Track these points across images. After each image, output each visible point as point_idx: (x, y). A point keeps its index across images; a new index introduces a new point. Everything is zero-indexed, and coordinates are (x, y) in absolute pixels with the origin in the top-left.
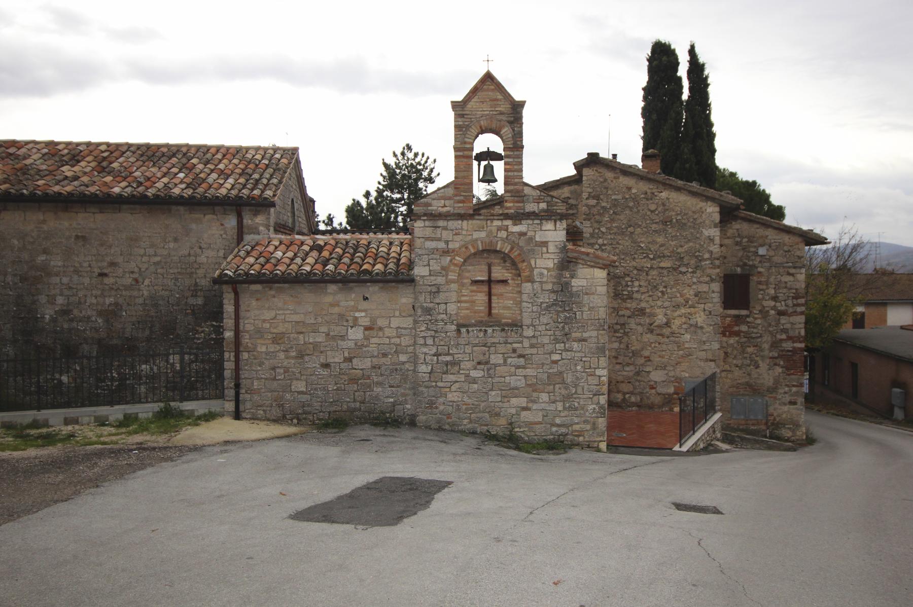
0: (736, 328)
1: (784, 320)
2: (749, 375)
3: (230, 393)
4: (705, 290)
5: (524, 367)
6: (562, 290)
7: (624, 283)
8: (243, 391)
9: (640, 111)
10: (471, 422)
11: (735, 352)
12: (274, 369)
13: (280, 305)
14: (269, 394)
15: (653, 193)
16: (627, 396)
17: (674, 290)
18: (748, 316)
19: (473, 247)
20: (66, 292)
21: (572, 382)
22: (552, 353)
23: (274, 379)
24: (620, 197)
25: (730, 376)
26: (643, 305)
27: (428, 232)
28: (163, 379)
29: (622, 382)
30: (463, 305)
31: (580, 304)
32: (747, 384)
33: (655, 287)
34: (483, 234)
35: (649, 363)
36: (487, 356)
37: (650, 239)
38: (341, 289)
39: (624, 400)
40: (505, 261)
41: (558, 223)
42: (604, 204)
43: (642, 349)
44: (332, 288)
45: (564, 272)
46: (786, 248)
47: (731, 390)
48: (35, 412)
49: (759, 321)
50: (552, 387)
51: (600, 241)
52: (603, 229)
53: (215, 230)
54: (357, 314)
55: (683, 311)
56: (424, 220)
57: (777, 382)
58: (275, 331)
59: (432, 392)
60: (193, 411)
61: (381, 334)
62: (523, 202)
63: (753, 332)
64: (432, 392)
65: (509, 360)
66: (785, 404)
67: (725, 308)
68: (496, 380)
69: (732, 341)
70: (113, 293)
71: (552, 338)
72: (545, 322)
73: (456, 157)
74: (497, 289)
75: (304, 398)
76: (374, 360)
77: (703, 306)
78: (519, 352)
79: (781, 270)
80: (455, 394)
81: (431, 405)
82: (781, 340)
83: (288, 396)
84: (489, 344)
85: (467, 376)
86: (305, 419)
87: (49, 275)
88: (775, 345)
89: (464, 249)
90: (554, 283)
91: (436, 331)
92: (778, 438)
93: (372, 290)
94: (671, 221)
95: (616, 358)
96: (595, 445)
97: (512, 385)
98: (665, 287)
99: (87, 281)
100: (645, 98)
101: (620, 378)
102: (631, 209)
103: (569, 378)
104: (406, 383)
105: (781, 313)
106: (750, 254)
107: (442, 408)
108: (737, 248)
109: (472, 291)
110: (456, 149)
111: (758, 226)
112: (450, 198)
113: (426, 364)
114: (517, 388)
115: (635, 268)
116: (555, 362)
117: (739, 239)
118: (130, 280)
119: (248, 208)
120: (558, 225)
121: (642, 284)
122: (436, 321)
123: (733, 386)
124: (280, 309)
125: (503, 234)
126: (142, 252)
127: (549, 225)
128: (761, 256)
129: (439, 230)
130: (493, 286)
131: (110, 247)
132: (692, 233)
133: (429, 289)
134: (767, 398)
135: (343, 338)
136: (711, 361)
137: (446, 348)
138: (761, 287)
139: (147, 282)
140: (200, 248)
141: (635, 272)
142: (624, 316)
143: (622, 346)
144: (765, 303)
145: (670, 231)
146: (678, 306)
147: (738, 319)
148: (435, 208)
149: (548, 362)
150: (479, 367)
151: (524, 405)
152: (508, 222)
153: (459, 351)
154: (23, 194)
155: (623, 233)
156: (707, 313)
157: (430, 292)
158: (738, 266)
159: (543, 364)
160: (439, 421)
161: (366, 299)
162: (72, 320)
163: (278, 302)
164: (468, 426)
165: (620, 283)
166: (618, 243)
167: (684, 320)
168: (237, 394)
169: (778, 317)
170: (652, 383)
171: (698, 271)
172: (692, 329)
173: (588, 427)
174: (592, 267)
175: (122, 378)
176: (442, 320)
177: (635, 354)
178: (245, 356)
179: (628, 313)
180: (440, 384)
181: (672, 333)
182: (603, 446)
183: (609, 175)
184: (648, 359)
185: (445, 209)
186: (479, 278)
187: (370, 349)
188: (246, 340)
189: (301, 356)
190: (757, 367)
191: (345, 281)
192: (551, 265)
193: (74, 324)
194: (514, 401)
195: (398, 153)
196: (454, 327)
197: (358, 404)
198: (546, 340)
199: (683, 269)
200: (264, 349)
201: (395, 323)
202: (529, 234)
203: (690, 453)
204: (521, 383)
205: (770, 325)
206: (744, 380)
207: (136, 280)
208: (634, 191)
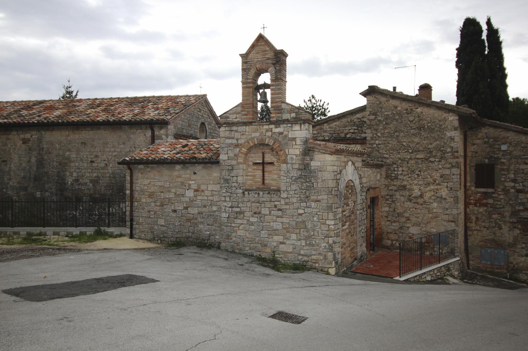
0: (485, 201)
1: (521, 196)
2: (494, 234)
3: (128, 224)
4: (447, 173)
5: (281, 217)
6: (305, 169)
7: (392, 169)
8: (135, 223)
9: (455, 64)
10: (250, 249)
11: (484, 218)
12: (149, 212)
13: (152, 176)
14: (147, 226)
15: (412, 109)
16: (394, 242)
17: (426, 173)
19: (252, 143)
20: (77, 171)
21: (311, 228)
22: (298, 208)
23: (149, 217)
24: (390, 113)
25: (480, 234)
26: (405, 183)
27: (227, 134)
28: (117, 216)
29: (391, 233)
30: (249, 177)
31: (316, 177)
32: (493, 240)
33: (413, 171)
34: (257, 134)
35: (408, 221)
36: (260, 209)
38: (182, 168)
39: (392, 245)
40: (273, 151)
41: (302, 125)
42: (379, 118)
43: (404, 212)
44: (178, 167)
45: (306, 157)
46: (523, 145)
47: (481, 243)
48: (42, 228)
49: (502, 197)
50: (298, 230)
51: (377, 142)
52: (379, 134)
53: (141, 137)
54: (190, 182)
55: (432, 187)
56: (225, 127)
57: (515, 239)
58: (150, 191)
59: (228, 229)
60: (112, 232)
61: (203, 194)
62: (281, 113)
63: (497, 204)
64: (228, 229)
65: (273, 212)
66: (522, 256)
67: (476, 187)
68: (265, 224)
69: (481, 210)
70: (96, 171)
71: (298, 199)
72: (294, 188)
73: (243, 88)
74: (268, 168)
75: (164, 229)
76: (199, 209)
77: (446, 184)
78: (278, 207)
79: (520, 161)
80: (241, 231)
81: (228, 237)
82: (519, 210)
83: (156, 227)
84: (261, 202)
85: (248, 221)
86: (164, 240)
87: (71, 162)
88: (514, 213)
89: (247, 144)
90: (300, 164)
91: (231, 193)
92: (516, 280)
93: (198, 168)
94: (424, 127)
95: (387, 217)
96: (326, 270)
97: (274, 228)
98: (420, 171)
99: (85, 165)
100: (458, 55)
101: (390, 230)
102: (397, 120)
103: (309, 226)
104: (216, 223)
105: (519, 191)
106: (495, 150)
107: (234, 239)
108: (486, 145)
109: (254, 169)
110: (243, 83)
111: (501, 130)
112: (239, 113)
113: (226, 212)
114: (277, 230)
115: (400, 159)
116: (301, 214)
117: (487, 140)
118: (104, 164)
119: (157, 125)
120: (302, 127)
121: (404, 169)
122: (231, 187)
124: (152, 179)
125: (269, 134)
126: (109, 150)
127: (297, 127)
128: (504, 151)
129: (233, 132)
130: (265, 166)
131: (95, 147)
132: (438, 135)
133: (228, 168)
134: (508, 251)
135: (183, 195)
136: (452, 222)
137: (237, 203)
138: (503, 173)
139: (111, 165)
140: (135, 147)
141: (400, 161)
142: (392, 190)
143: (391, 210)
144: (507, 184)
145: (423, 134)
146: (428, 184)
147: (486, 195)
148: (231, 119)
149: (296, 214)
150: (255, 215)
151: (282, 241)
152: (272, 126)
153: (244, 205)
154: (59, 122)
155: (392, 137)
156: (449, 189)
157: (228, 170)
158: (486, 158)
159: (293, 216)
160: (232, 247)
161: (195, 173)
162: (79, 184)
163: (151, 175)
164: (249, 251)
165: (389, 169)
166: (388, 143)
167: (432, 193)
168: (132, 225)
169: (517, 194)
170: (411, 235)
171: (443, 161)
172: (438, 199)
173: (322, 258)
174: (324, 153)
175: (100, 215)
176: (235, 187)
177: (399, 215)
178: (136, 204)
179: (395, 188)
180: (233, 225)
181: (425, 202)
182: (332, 271)
183: (383, 99)
184: (408, 219)
185: (237, 120)
186: (258, 161)
187: (197, 203)
188: (136, 195)
189: (162, 205)
190: (500, 228)
191: (183, 163)
192: (298, 153)
193: (80, 187)
194: (276, 238)
195: (307, 100)
196: (241, 191)
197: (191, 234)
198: (295, 200)
199: (432, 159)
200: (144, 201)
201: (210, 188)
202: (285, 133)
203: (407, 281)
204: (280, 227)
205: (510, 199)
206: (490, 237)
207: (106, 164)
208: (399, 109)
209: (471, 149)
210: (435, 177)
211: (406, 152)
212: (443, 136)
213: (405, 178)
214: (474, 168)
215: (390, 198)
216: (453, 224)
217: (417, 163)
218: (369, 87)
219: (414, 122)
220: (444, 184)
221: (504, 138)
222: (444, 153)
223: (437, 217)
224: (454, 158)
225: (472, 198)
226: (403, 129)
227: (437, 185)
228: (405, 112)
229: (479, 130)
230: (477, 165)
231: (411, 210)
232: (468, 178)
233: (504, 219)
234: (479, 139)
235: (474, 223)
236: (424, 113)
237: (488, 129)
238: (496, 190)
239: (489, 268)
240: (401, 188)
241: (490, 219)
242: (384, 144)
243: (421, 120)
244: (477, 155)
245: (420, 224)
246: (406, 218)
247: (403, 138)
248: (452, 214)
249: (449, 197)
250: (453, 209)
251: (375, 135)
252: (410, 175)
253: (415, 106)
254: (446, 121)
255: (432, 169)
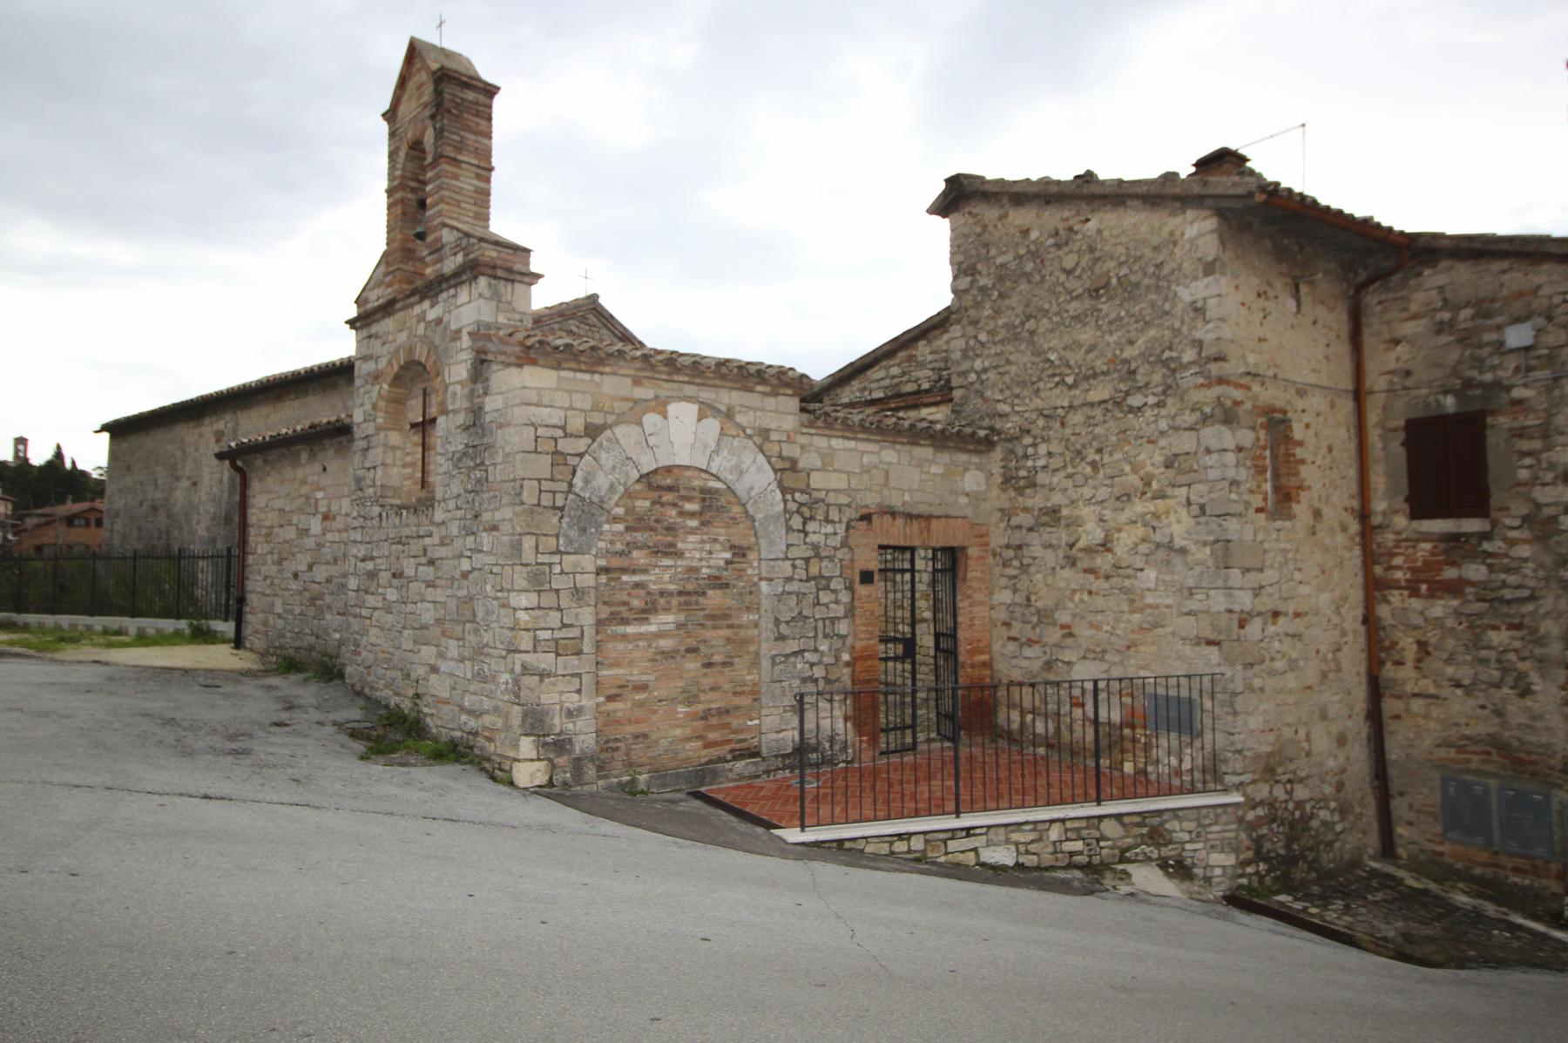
2: (1499, 713)
4: (1187, 448)
11: (1451, 643)
15: (1071, 229)
17: (1118, 456)
18: (1485, 536)
24: (1008, 257)
25: (1436, 712)
26: (1057, 499)
32: (1494, 741)
33: (1079, 453)
35: (1069, 641)
37: (1067, 339)
47: (1442, 753)
51: (978, 364)
52: (983, 337)
55: (1139, 507)
63: (1504, 585)
69: (1438, 608)
77: (1184, 490)
94: (1107, 285)
95: (1007, 624)
98: (1099, 451)
102: (1028, 277)
108: (1445, 339)
111: (1505, 264)
115: (1041, 413)
117: (1446, 316)
123: (1446, 743)
136: (1210, 643)
138: (1525, 445)
141: (1041, 422)
142: (1019, 527)
144: (1542, 495)
146: (1125, 497)
155: (1017, 338)
156: (1195, 510)
158: (1446, 393)
165: (1012, 451)
166: (1008, 362)
167: (1140, 531)
171: (1170, 401)
177: (1044, 617)
181: (1117, 567)
190: (1526, 692)
199: (1135, 401)
206: (1481, 729)
209: (1381, 363)
210: (1149, 468)
211: (1057, 384)
212: (1167, 307)
213: (1055, 480)
214: (1402, 435)
215: (1016, 557)
216: (1213, 654)
217: (1089, 421)
218: (948, 181)
219: (1078, 272)
220: (1177, 491)
221: (1519, 295)
222: (1174, 371)
223: (1155, 626)
224: (1209, 386)
225: (1398, 561)
226: (1046, 306)
227: (1154, 498)
228: (1051, 241)
229: (1412, 282)
230: (1412, 426)
231: (1077, 597)
232: (1378, 480)
233: (1538, 651)
234: (1415, 317)
235: (1409, 664)
236: (1106, 233)
237: (1450, 269)
238: (1494, 524)
239: (1480, 864)
240: (1045, 519)
241: (1477, 647)
242: (996, 367)
243: (1098, 259)
244: (1409, 382)
245: (1104, 651)
246: (1062, 627)
247: (1049, 335)
248: (1207, 612)
249: (1196, 542)
250: (1212, 593)
251: (972, 343)
252: (1070, 470)
253: (1078, 214)
254: (1175, 243)
255: (1137, 438)
